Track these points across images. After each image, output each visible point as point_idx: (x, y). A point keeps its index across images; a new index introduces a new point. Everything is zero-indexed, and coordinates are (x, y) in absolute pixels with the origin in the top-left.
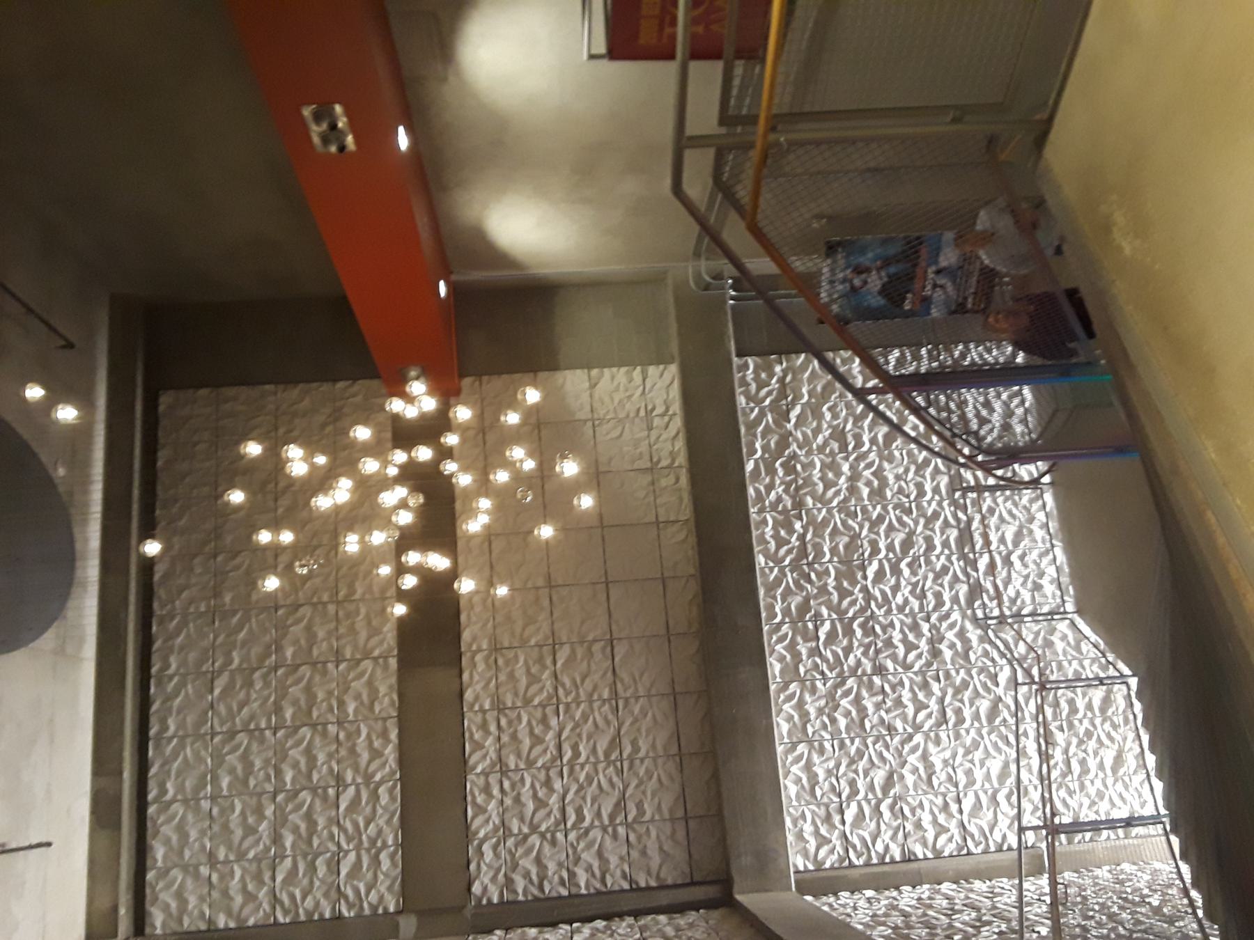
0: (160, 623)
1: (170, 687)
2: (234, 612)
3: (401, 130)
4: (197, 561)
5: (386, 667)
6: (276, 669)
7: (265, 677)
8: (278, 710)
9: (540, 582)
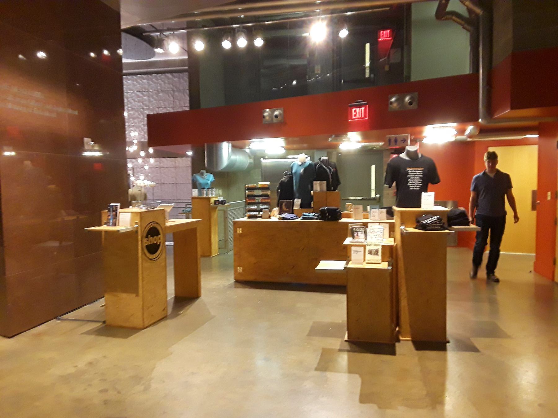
0: (155, 76)
1: (139, 80)
2: (157, 97)
3: (383, 143)
4: (171, 85)
5: (142, 138)
6: (143, 108)
7: (140, 106)
8: (133, 109)
9: (162, 181)
